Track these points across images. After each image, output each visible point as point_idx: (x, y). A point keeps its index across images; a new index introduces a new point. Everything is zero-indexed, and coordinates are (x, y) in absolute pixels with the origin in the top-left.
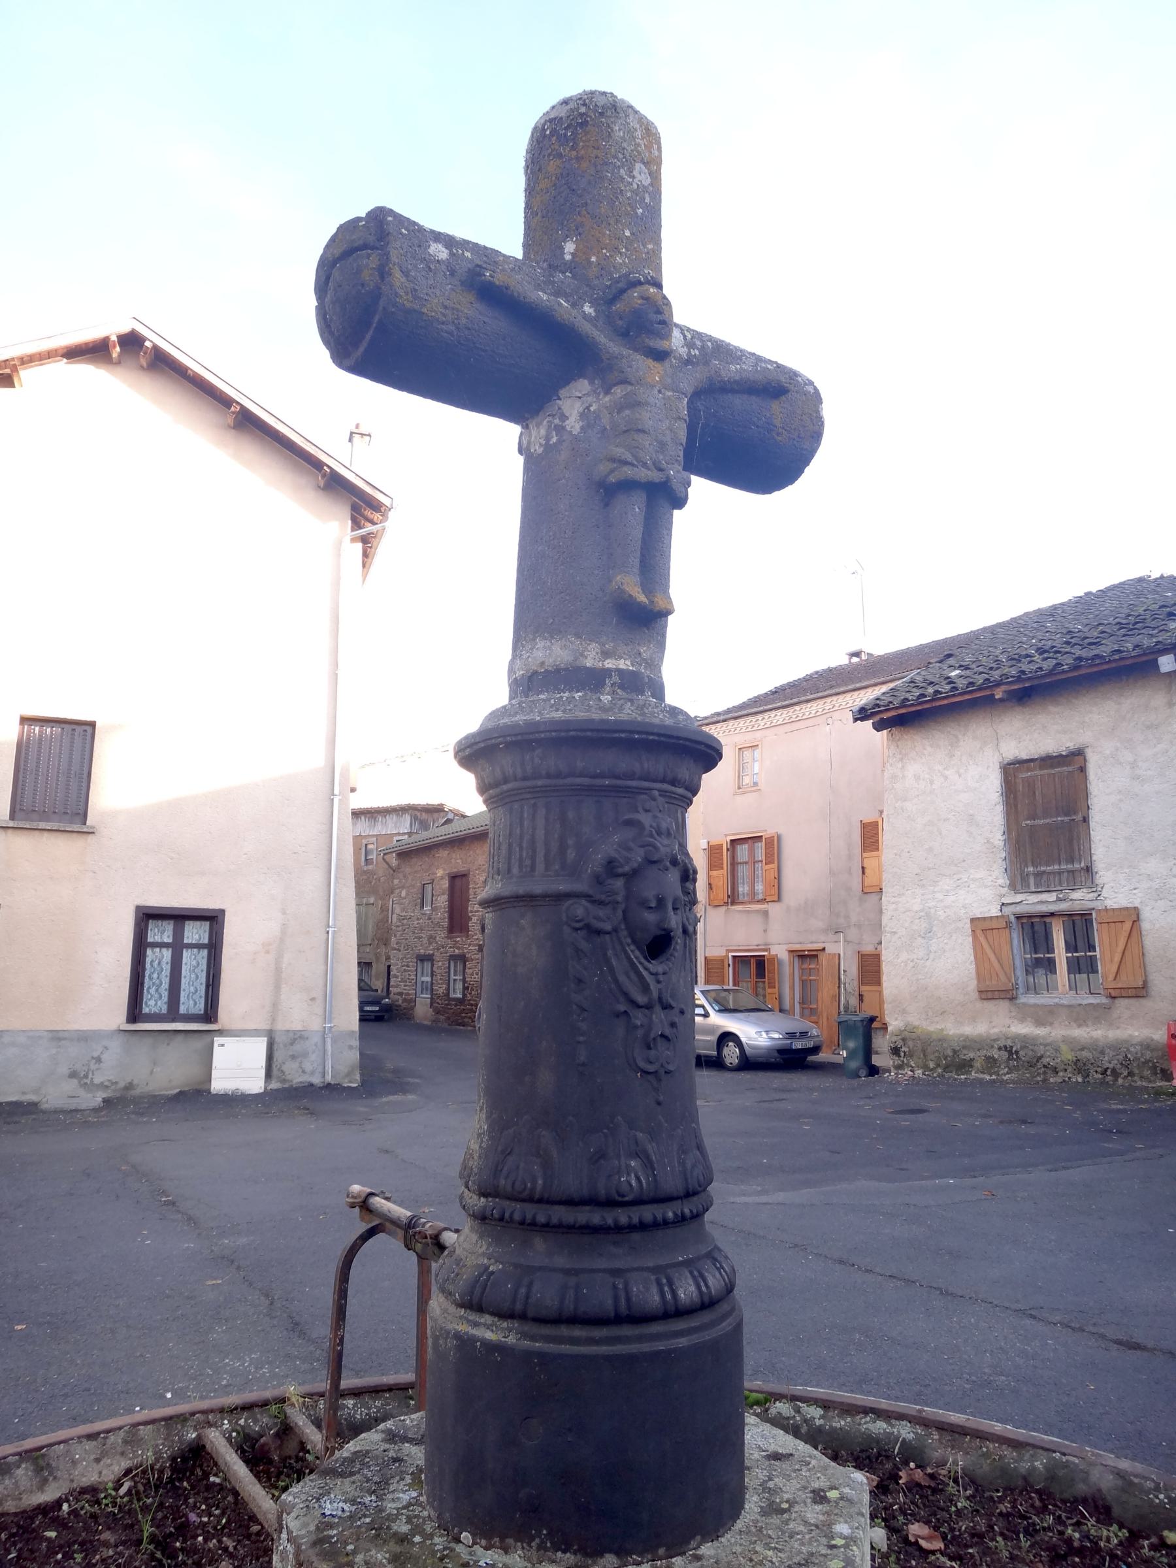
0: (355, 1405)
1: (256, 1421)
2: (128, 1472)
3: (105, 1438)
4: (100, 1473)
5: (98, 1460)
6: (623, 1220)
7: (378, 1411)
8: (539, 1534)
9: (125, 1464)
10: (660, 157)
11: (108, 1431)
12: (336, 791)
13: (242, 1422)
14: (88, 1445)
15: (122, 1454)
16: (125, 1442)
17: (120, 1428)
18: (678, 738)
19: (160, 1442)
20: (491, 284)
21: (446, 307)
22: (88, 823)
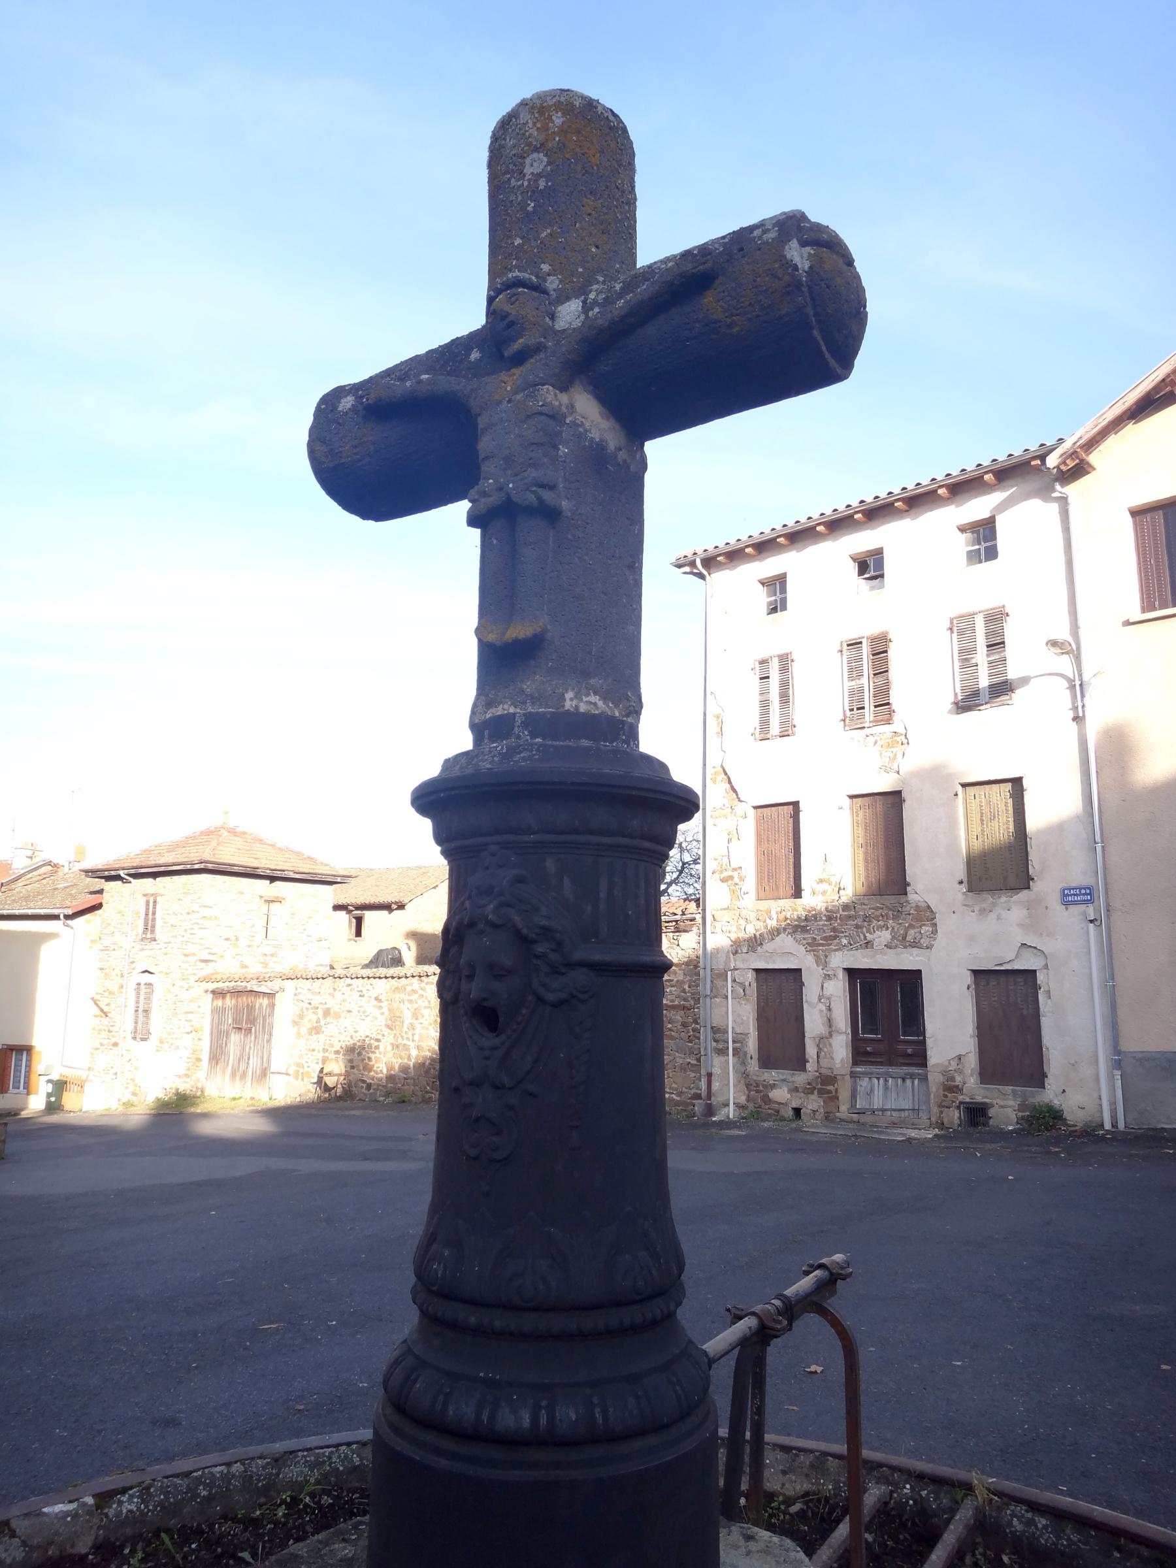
0: (1045, 1527)
1: (937, 1498)
2: (807, 1494)
3: (796, 1455)
4: (783, 1485)
5: (784, 1473)
6: (498, 1324)
7: (1068, 1546)
8: (153, 1511)
9: (806, 1486)
10: (583, 97)
11: (800, 1450)
12: (1098, 839)
13: (924, 1493)
14: (780, 1455)
15: (807, 1475)
16: (812, 1466)
17: (812, 1451)
18: (669, 794)
19: (843, 1479)
20: (369, 405)
21: (355, 447)
22: (1088, 881)
